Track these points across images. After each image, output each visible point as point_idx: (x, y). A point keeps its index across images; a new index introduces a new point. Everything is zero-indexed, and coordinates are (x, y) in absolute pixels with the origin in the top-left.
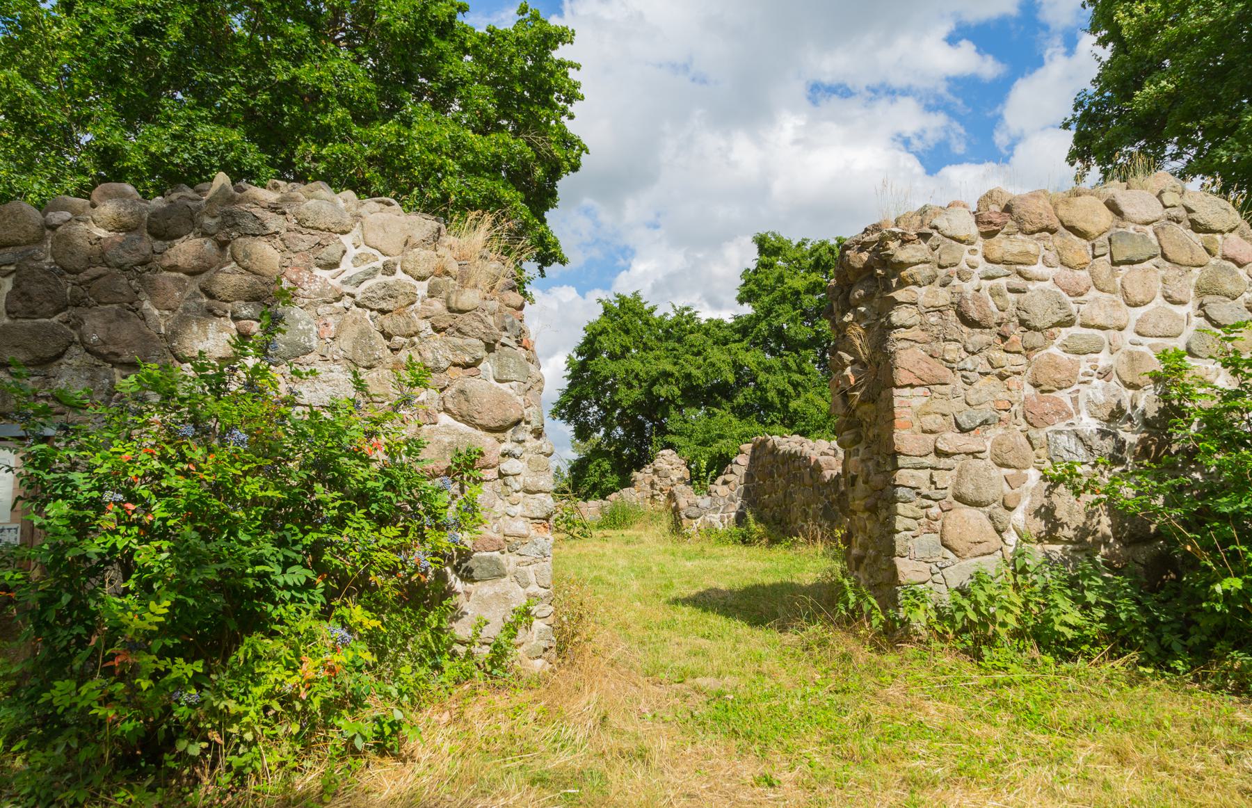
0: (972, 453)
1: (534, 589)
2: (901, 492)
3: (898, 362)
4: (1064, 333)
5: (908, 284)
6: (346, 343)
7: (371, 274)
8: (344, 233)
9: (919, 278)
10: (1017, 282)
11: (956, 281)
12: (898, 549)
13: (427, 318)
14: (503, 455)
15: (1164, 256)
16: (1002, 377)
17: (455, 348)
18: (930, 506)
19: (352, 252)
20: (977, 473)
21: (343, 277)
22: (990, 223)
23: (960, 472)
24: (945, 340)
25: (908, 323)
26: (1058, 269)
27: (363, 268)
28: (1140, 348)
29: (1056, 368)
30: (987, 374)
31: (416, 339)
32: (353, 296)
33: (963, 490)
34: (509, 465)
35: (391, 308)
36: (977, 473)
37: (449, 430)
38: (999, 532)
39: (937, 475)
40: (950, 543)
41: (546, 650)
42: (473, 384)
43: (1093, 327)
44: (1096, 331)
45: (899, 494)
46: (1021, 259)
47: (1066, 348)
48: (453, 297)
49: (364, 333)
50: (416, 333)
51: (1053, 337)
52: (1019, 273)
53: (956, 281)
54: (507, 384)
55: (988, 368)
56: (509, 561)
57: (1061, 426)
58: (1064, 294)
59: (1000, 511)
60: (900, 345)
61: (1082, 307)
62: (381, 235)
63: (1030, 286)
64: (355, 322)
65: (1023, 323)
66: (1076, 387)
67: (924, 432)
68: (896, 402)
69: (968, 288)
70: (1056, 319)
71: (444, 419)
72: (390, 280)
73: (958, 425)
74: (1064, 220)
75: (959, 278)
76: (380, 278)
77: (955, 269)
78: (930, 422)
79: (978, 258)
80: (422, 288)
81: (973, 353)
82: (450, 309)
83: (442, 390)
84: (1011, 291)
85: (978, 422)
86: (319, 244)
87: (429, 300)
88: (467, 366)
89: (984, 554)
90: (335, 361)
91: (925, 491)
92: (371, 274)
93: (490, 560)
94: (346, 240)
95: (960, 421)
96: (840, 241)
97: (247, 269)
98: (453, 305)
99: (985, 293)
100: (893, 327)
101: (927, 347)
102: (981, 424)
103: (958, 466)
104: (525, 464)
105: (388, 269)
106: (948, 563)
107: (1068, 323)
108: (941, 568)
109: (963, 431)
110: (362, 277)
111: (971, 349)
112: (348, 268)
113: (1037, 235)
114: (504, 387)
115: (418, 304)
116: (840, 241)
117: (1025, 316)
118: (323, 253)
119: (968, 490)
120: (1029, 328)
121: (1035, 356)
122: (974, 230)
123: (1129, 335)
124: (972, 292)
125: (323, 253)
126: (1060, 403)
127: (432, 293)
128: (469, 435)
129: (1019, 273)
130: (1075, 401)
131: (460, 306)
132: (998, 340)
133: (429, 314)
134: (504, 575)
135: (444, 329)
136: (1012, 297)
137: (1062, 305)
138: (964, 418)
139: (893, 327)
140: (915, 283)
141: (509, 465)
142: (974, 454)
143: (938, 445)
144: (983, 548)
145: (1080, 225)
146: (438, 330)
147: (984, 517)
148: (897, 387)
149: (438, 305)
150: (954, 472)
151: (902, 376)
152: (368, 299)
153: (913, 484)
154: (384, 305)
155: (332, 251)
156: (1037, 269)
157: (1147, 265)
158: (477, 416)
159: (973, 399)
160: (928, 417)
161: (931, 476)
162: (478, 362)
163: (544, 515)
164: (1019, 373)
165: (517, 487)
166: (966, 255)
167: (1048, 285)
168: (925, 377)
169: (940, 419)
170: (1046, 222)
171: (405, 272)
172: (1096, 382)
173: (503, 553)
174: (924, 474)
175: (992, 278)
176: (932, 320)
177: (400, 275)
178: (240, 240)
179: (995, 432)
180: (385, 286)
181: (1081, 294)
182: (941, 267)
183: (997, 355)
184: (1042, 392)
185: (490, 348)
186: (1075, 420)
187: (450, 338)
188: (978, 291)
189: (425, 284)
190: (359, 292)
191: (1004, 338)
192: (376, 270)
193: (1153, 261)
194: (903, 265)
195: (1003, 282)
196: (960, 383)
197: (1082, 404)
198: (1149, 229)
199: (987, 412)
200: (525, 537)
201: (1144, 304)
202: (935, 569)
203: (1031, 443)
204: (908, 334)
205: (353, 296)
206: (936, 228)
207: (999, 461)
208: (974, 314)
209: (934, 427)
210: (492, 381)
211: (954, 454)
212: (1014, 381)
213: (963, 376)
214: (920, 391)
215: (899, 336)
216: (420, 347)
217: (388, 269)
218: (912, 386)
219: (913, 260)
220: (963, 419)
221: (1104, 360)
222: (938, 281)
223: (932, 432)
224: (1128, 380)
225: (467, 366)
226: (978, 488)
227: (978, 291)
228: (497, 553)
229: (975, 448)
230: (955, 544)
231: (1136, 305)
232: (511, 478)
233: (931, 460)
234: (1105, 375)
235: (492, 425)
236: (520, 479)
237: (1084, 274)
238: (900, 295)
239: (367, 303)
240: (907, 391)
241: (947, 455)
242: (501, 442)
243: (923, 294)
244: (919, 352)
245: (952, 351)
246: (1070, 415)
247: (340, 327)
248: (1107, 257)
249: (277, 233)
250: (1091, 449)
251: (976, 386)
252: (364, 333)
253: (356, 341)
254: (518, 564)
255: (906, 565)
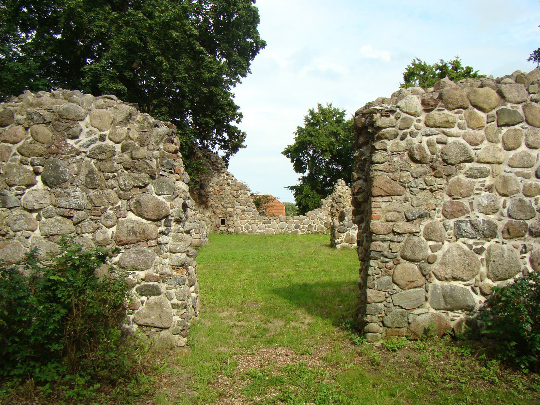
0: (413, 233)
1: (175, 301)
2: (372, 254)
3: (374, 183)
4: (468, 165)
5: (382, 139)
6: (82, 177)
7: (93, 142)
8: (81, 120)
9: (388, 136)
10: (442, 137)
11: (409, 137)
12: (369, 284)
13: (121, 163)
14: (160, 233)
15: (527, 122)
16: (432, 191)
17: (135, 179)
18: (388, 262)
19: (86, 130)
20: (414, 245)
21: (80, 143)
22: (429, 105)
23: (405, 244)
24: (401, 170)
25: (380, 161)
26: (467, 130)
27: (90, 138)
28: (510, 174)
29: (461, 185)
30: (425, 189)
31: (115, 174)
32: (85, 153)
33: (406, 253)
34: (163, 239)
35: (104, 158)
36: (414, 245)
37: (132, 221)
38: (424, 276)
39: (393, 245)
40: (397, 282)
41: (181, 331)
42: (144, 197)
43: (484, 163)
44: (486, 166)
45: (371, 255)
46: (444, 125)
47: (468, 175)
48: (134, 153)
49: (91, 172)
50: (116, 171)
51: (460, 168)
52: (444, 133)
53: (409, 137)
54: (162, 196)
55: (425, 186)
56: (163, 287)
57: (462, 218)
58: (468, 145)
59: (425, 264)
60: (378, 173)
61: (478, 152)
62: (99, 121)
63: (450, 140)
64: (86, 166)
65: (444, 161)
66: (472, 196)
67: (387, 221)
68: (373, 204)
69: (415, 141)
70: (462, 159)
71: (131, 216)
72: (103, 144)
73: (406, 217)
74: (472, 101)
75: (410, 135)
76: (99, 143)
77: (408, 131)
78: (390, 215)
79: (421, 124)
80: (118, 148)
81: (417, 178)
82: (132, 158)
83: (128, 200)
84: (439, 143)
85: (417, 216)
86: (69, 127)
87: (122, 154)
88: (140, 187)
89: (416, 287)
90: (77, 186)
91: (385, 253)
92: (93, 142)
93: (153, 286)
94: (82, 124)
95: (407, 215)
96: (469, 70)
97: (37, 141)
98: (134, 156)
99: (424, 144)
100: (373, 163)
101: (391, 174)
102: (418, 217)
103: (404, 240)
104: (171, 238)
105: (102, 138)
106: (395, 292)
107: (470, 160)
108: (391, 295)
109: (408, 220)
110: (89, 143)
111: (415, 176)
112: (84, 139)
113: (456, 111)
114: (161, 198)
115: (116, 156)
116: (469, 70)
117: (445, 158)
118: (71, 132)
119: (408, 253)
120: (448, 164)
121: (451, 180)
122: (420, 108)
123: (504, 167)
124: (417, 144)
125: (71, 132)
126: (463, 205)
127: (124, 150)
128: (142, 223)
129: (444, 133)
130: (471, 204)
131: (137, 156)
132: (431, 171)
133: (121, 161)
134: (160, 294)
135: (129, 169)
136: (440, 146)
137: (466, 151)
138: (410, 214)
139: (373, 163)
140: (386, 138)
141: (163, 239)
142: (414, 234)
143: (394, 229)
144: (414, 284)
145: (481, 105)
146: (127, 169)
147: (416, 267)
148: (374, 197)
149: (126, 156)
150: (402, 244)
151: (375, 191)
152: (93, 154)
153: (380, 250)
154: (100, 157)
155: (75, 129)
156: (455, 130)
157: (517, 127)
158: (145, 214)
159: (415, 202)
160: (390, 213)
161: (390, 246)
162: (146, 185)
163: (180, 264)
164: (441, 189)
165: (166, 250)
166: (415, 123)
167: (461, 140)
168: (389, 191)
169: (397, 214)
170: (460, 104)
171: (111, 140)
172: (483, 193)
173: (159, 283)
174: (386, 245)
175: (429, 135)
176: (395, 159)
177: (108, 142)
178: (34, 126)
179: (426, 222)
180: (100, 147)
181: (478, 145)
182: (400, 129)
183: (430, 178)
184: (454, 199)
185: (152, 177)
186: (471, 214)
187: (132, 174)
188: (421, 143)
189: (120, 145)
190: (88, 150)
191: (434, 169)
192: (96, 139)
193: (521, 125)
194: (379, 128)
195: (434, 138)
196: (407, 194)
197: (475, 205)
198: (520, 106)
199: (423, 210)
200: (170, 275)
201: (513, 149)
202: (388, 295)
203: (445, 227)
204: (381, 167)
205: (85, 153)
206: (398, 107)
207: (427, 237)
208: (417, 157)
209: (393, 219)
210: (155, 195)
211: (403, 233)
212: (439, 194)
213: (410, 190)
214: (386, 199)
215: (376, 168)
216: (118, 178)
217: (102, 138)
218: (382, 196)
219: (384, 126)
220: (409, 215)
221: (488, 181)
222: (399, 137)
223: (391, 221)
224: (501, 192)
225: (140, 187)
226: (414, 253)
227: (421, 143)
228: (156, 283)
229: (414, 230)
230: (399, 282)
231: (509, 149)
232: (163, 245)
233: (391, 236)
234: (489, 189)
235: (153, 218)
236: (168, 246)
237: (482, 132)
238: (378, 145)
239: (92, 156)
240: (378, 199)
241: (399, 234)
242: (159, 226)
243: (389, 144)
244: (387, 177)
245: (405, 176)
246: (468, 212)
247: (79, 169)
248: (495, 123)
249: (50, 122)
250: (478, 231)
251: (418, 196)
252: (91, 172)
253: (87, 176)
254: (167, 289)
255: (372, 293)
